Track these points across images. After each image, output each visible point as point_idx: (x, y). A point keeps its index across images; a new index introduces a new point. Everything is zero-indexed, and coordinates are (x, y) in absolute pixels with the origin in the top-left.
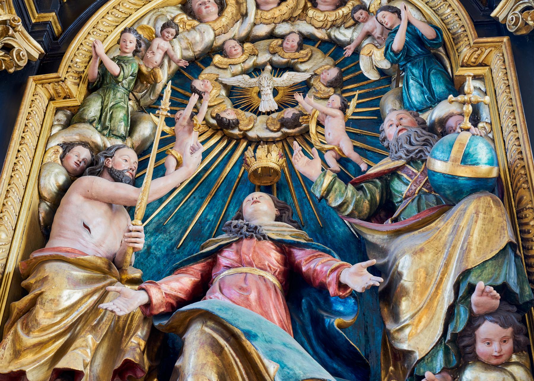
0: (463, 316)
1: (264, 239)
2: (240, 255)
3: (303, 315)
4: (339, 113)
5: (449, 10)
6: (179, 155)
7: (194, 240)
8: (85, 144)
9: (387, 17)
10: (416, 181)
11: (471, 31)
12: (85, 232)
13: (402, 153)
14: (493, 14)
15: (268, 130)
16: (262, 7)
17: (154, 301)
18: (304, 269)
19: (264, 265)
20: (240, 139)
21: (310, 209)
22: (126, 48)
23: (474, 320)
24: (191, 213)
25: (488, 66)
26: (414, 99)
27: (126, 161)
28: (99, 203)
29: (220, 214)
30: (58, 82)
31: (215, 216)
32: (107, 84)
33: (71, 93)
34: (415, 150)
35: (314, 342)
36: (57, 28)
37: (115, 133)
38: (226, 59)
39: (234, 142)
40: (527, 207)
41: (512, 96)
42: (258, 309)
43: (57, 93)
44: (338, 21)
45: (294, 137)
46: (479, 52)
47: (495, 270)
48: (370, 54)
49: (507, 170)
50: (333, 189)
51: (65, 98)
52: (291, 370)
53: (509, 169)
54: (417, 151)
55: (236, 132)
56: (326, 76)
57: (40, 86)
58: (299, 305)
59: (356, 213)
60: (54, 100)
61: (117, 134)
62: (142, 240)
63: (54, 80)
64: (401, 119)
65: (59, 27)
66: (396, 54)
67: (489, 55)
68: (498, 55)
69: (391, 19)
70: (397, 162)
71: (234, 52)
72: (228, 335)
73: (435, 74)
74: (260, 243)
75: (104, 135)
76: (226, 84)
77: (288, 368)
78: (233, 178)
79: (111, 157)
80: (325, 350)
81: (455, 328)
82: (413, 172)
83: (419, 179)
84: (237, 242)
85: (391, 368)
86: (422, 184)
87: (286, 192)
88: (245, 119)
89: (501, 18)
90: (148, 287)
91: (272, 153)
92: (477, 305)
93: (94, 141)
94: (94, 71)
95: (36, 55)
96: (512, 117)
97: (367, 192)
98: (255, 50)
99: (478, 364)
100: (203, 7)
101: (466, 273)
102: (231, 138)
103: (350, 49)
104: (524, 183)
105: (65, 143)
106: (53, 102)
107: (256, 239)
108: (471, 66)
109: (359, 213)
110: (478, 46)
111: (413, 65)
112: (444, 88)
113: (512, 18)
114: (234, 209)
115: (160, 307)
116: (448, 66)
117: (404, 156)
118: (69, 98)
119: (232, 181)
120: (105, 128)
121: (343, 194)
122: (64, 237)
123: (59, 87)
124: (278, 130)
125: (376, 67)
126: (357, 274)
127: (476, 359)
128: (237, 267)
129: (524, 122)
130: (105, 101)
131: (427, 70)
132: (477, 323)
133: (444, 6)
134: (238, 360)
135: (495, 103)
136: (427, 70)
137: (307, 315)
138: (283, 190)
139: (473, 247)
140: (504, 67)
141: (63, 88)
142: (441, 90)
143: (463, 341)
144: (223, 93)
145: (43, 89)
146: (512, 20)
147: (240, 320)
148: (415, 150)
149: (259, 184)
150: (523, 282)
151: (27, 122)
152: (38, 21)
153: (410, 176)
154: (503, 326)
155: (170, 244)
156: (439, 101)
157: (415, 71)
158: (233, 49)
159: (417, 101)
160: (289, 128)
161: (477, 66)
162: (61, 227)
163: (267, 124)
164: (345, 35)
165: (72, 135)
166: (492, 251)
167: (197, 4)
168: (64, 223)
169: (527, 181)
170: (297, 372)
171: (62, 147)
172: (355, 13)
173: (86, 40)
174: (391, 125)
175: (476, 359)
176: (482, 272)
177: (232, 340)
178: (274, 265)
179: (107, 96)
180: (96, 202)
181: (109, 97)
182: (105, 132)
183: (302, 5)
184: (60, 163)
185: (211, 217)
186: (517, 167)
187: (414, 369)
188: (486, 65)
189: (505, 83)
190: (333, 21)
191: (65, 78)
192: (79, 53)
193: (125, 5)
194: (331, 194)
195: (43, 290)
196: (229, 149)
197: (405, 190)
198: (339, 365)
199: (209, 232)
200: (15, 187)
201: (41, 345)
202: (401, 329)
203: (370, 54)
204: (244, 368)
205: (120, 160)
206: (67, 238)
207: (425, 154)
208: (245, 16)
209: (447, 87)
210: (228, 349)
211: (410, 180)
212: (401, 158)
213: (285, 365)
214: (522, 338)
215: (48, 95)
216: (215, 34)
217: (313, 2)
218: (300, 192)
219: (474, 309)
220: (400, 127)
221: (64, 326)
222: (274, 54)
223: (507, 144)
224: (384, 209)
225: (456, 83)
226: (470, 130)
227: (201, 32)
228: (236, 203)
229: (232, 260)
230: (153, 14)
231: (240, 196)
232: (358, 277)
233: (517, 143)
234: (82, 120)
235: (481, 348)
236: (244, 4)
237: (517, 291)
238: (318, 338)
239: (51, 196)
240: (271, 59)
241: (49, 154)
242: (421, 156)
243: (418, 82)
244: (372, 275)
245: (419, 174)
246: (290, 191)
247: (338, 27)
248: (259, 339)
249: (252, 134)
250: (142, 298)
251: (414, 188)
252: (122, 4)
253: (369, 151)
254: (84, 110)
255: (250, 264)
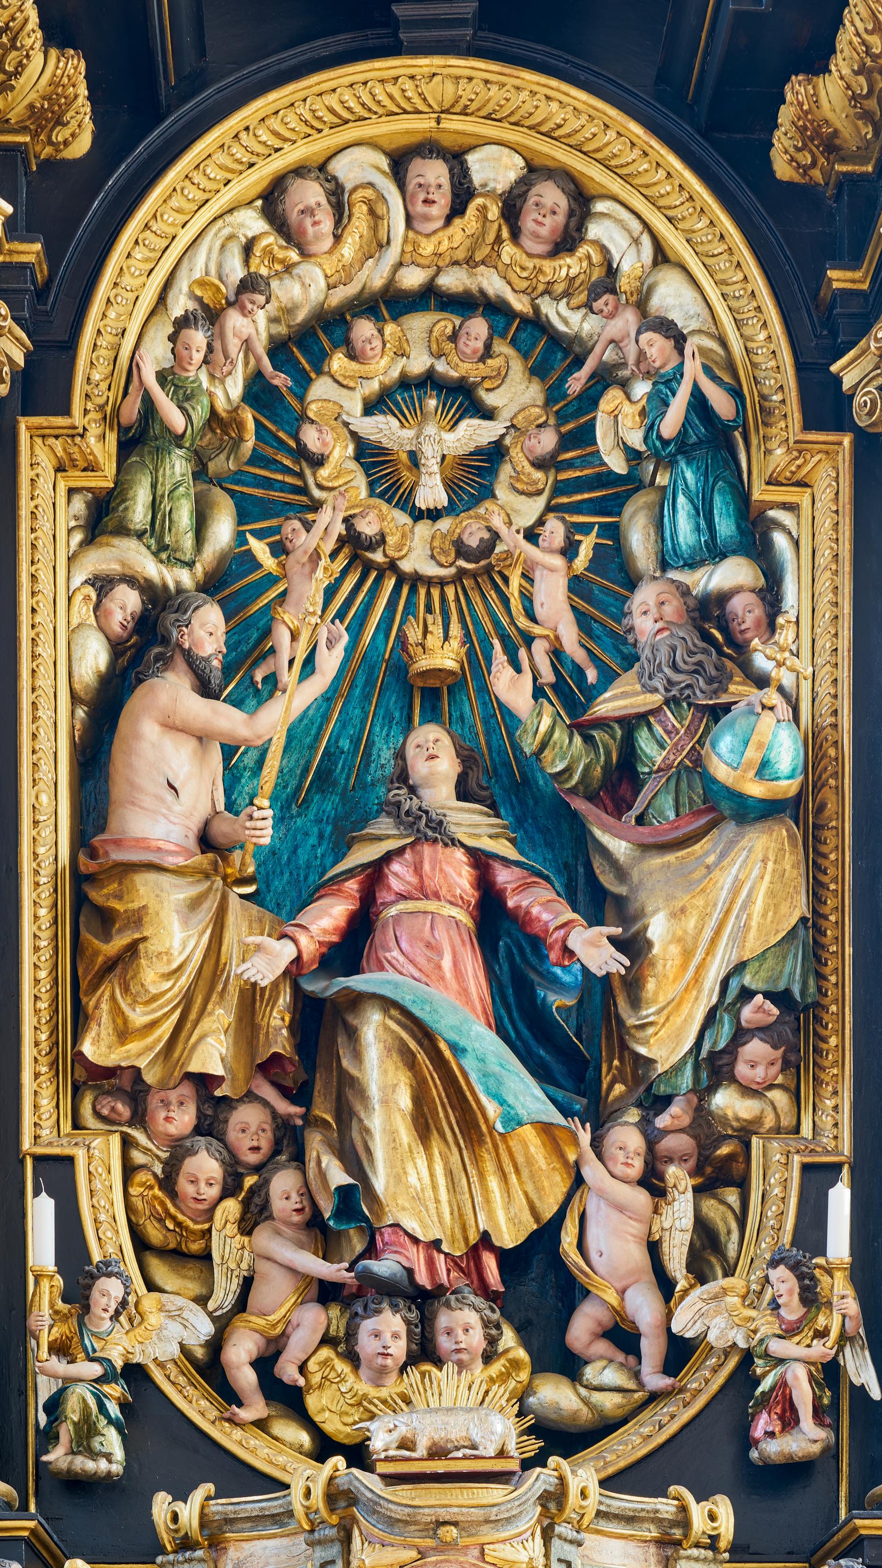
0: (727, 1026)
1: (454, 844)
2: (421, 877)
3: (501, 968)
4: (558, 561)
5: (762, 336)
6: (296, 623)
7: (323, 792)
8: (131, 580)
9: (657, 346)
10: (676, 744)
11: (796, 417)
12: (169, 796)
13: (658, 683)
14: (834, 368)
15: (433, 562)
16: (417, 225)
17: (305, 957)
18: (510, 904)
19: (454, 896)
20: (385, 570)
21: (501, 742)
22: (190, 364)
23: (740, 1036)
24: (313, 732)
25: (809, 486)
26: (681, 539)
27: (211, 634)
28: (185, 736)
29: (359, 740)
30: (73, 436)
31: (351, 741)
32: (156, 439)
33: (97, 463)
34: (680, 683)
35: (515, 1015)
36: (42, 271)
37: (178, 555)
38: (354, 365)
39: (374, 575)
40: (830, 825)
41: (838, 581)
42: (454, 985)
43: (73, 460)
44: (556, 286)
45: (474, 575)
46: (799, 462)
47: (777, 964)
48: (616, 412)
49: (810, 735)
50: (551, 743)
51: (85, 470)
52: (512, 1108)
53: (813, 734)
54: (683, 685)
55: (378, 557)
56: (534, 446)
57: (39, 441)
58: (495, 950)
59: (581, 788)
60: (65, 471)
61: (182, 558)
62: (270, 831)
63: (65, 431)
64: (663, 603)
65: (46, 272)
66: (666, 443)
67: (816, 469)
68: (831, 470)
69: (662, 350)
70: (648, 695)
71: (370, 353)
72: (420, 1036)
73: (722, 492)
74: (448, 851)
75: (162, 562)
76: (356, 433)
77: (509, 1106)
78: (375, 658)
79: (187, 626)
80: (530, 1029)
81: (715, 1043)
82: (674, 726)
83: (682, 743)
84: (412, 845)
85: (616, 1062)
86: (684, 753)
87: (462, 700)
88: (394, 530)
89: (847, 382)
90: (297, 935)
91: (451, 641)
92: (747, 1022)
93: (147, 576)
94: (131, 410)
95: (20, 359)
96: (833, 632)
97: (601, 750)
98: (405, 345)
99: (733, 1087)
100: (308, 222)
101: (740, 967)
102: (368, 566)
103: (578, 380)
104: (831, 776)
105: (96, 578)
106: (64, 474)
107: (441, 844)
108: (782, 485)
109: (586, 788)
110: (800, 449)
111: (688, 463)
112: (734, 528)
113: (865, 402)
114: (382, 729)
115: (312, 964)
116: (744, 465)
117: (662, 690)
118: (93, 471)
119: (374, 667)
120: (163, 547)
121: (565, 753)
122: (141, 808)
123: (76, 449)
124: (451, 565)
125: (624, 443)
126: (593, 943)
127: (733, 1080)
128: (417, 899)
129: (849, 651)
130: (159, 486)
131: (711, 480)
132: (744, 1039)
133: (755, 320)
134: (435, 1076)
135: (810, 582)
136: (711, 480)
137: (506, 968)
138: (457, 697)
139: (754, 924)
140: (834, 508)
141: (82, 451)
142: (729, 533)
143: (721, 1058)
144: (351, 450)
145: (46, 449)
146: (866, 406)
147: (443, 1022)
148: (680, 683)
149: (421, 684)
150: (808, 971)
151: (33, 536)
152: (8, 259)
153: (668, 733)
154: (775, 1047)
155: (284, 796)
156: (724, 556)
157: (689, 475)
158: (368, 347)
159: (686, 544)
160: (468, 561)
161: (793, 485)
162: (132, 784)
163: (432, 549)
164: (566, 322)
165: (103, 559)
166: (777, 932)
167: (296, 210)
168: (137, 780)
169: (837, 772)
170: (519, 1112)
171: (93, 585)
172: (595, 300)
173: (104, 322)
174: (645, 613)
175: (733, 1080)
176: (760, 966)
177: (426, 1042)
178: (467, 894)
179: (161, 472)
180: (180, 734)
181: (164, 475)
182: (164, 556)
183: (491, 237)
184: (95, 624)
185: (345, 744)
186: (827, 740)
187: (652, 1083)
188: (806, 485)
189: (832, 548)
190: (548, 283)
191: (85, 429)
192: (98, 359)
193: (166, 217)
194: (546, 752)
195: (145, 934)
196: (366, 588)
197: (659, 757)
198: (547, 1052)
199: (344, 776)
200: (43, 694)
201: (153, 1025)
202: (643, 1027)
203: (616, 412)
204: (444, 1089)
205: (202, 633)
206: (141, 808)
207: (695, 694)
208: (383, 245)
209: (739, 527)
210: (422, 1057)
211: (668, 741)
212: (656, 690)
213: (505, 1101)
214: (793, 1058)
215: (54, 462)
216: (328, 285)
217: (512, 221)
218: (484, 703)
219: (743, 1023)
220: (659, 625)
221: (180, 992)
222: (439, 355)
223: (817, 683)
224: (620, 782)
225: (752, 510)
226: (775, 710)
227: (303, 284)
228: (383, 718)
229: (409, 883)
230: (216, 235)
231: (388, 702)
232: (594, 950)
233: (832, 691)
234: (122, 530)
235: (742, 1070)
236: (385, 222)
237: (799, 999)
238: (521, 1009)
239: (90, 695)
240: (432, 366)
241: (75, 609)
242: (689, 696)
243: (692, 501)
244: (613, 949)
245: (682, 732)
246: (469, 699)
247: (558, 299)
248: (468, 1056)
249: (406, 566)
250: (286, 952)
251: (672, 757)
252: (162, 216)
253: (596, 621)
254: (126, 509)
255: (437, 896)
